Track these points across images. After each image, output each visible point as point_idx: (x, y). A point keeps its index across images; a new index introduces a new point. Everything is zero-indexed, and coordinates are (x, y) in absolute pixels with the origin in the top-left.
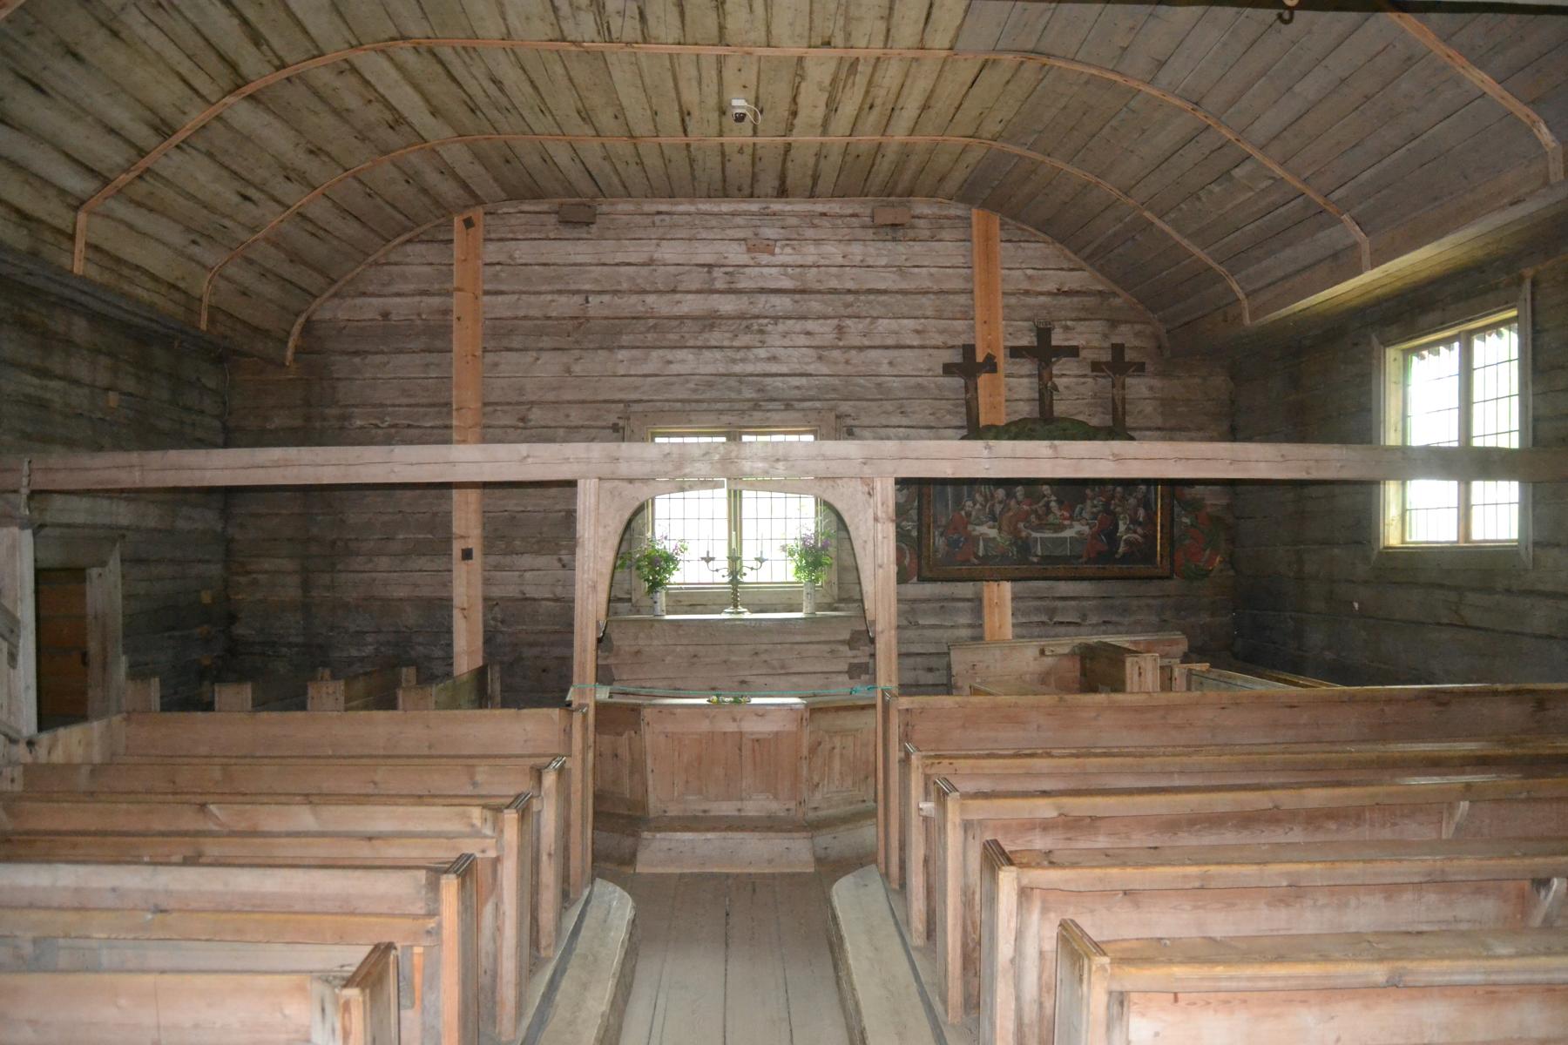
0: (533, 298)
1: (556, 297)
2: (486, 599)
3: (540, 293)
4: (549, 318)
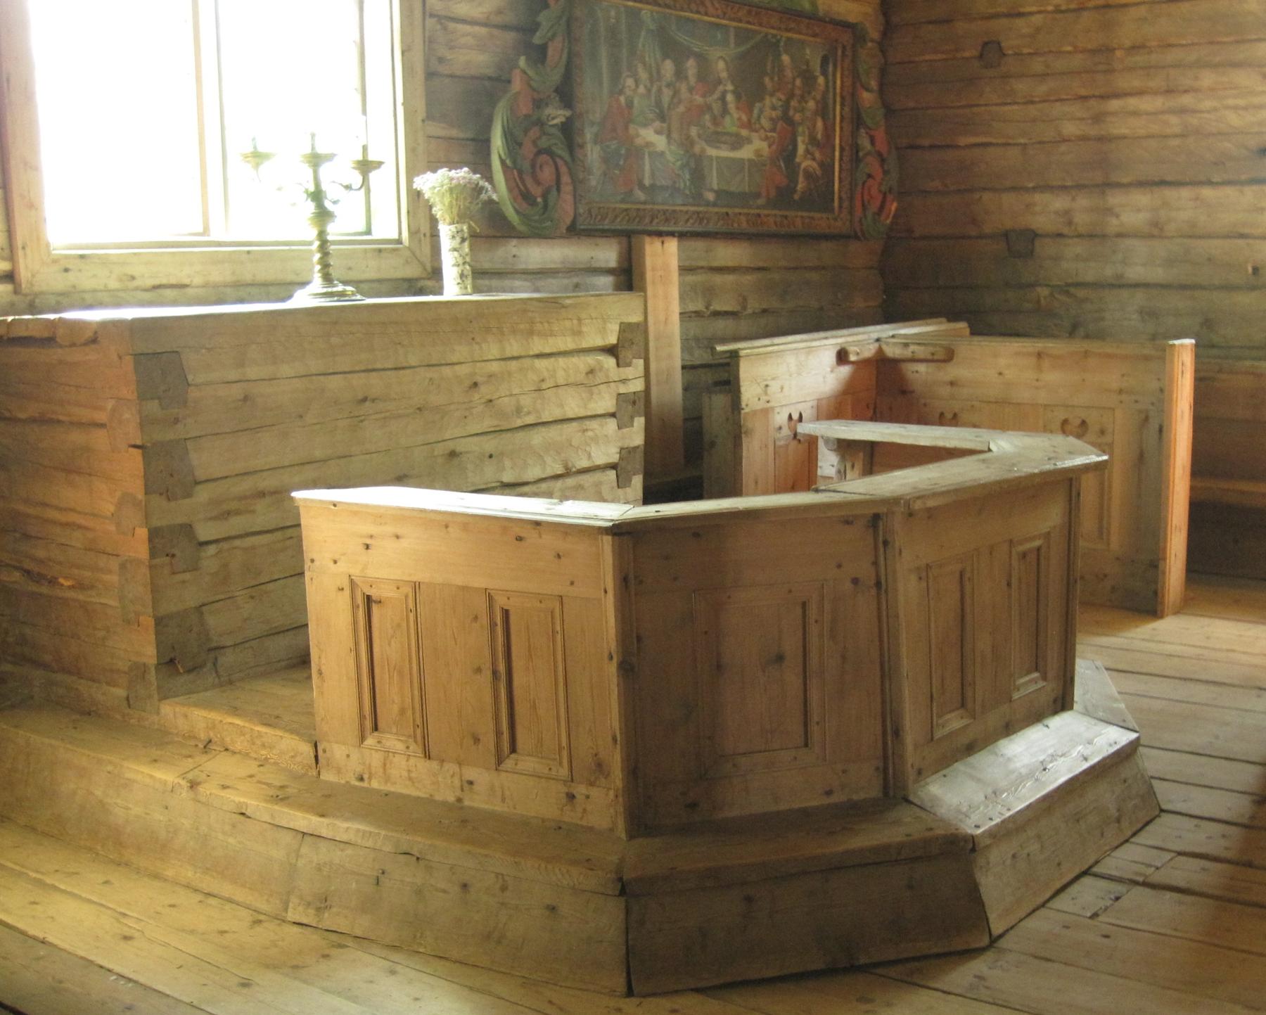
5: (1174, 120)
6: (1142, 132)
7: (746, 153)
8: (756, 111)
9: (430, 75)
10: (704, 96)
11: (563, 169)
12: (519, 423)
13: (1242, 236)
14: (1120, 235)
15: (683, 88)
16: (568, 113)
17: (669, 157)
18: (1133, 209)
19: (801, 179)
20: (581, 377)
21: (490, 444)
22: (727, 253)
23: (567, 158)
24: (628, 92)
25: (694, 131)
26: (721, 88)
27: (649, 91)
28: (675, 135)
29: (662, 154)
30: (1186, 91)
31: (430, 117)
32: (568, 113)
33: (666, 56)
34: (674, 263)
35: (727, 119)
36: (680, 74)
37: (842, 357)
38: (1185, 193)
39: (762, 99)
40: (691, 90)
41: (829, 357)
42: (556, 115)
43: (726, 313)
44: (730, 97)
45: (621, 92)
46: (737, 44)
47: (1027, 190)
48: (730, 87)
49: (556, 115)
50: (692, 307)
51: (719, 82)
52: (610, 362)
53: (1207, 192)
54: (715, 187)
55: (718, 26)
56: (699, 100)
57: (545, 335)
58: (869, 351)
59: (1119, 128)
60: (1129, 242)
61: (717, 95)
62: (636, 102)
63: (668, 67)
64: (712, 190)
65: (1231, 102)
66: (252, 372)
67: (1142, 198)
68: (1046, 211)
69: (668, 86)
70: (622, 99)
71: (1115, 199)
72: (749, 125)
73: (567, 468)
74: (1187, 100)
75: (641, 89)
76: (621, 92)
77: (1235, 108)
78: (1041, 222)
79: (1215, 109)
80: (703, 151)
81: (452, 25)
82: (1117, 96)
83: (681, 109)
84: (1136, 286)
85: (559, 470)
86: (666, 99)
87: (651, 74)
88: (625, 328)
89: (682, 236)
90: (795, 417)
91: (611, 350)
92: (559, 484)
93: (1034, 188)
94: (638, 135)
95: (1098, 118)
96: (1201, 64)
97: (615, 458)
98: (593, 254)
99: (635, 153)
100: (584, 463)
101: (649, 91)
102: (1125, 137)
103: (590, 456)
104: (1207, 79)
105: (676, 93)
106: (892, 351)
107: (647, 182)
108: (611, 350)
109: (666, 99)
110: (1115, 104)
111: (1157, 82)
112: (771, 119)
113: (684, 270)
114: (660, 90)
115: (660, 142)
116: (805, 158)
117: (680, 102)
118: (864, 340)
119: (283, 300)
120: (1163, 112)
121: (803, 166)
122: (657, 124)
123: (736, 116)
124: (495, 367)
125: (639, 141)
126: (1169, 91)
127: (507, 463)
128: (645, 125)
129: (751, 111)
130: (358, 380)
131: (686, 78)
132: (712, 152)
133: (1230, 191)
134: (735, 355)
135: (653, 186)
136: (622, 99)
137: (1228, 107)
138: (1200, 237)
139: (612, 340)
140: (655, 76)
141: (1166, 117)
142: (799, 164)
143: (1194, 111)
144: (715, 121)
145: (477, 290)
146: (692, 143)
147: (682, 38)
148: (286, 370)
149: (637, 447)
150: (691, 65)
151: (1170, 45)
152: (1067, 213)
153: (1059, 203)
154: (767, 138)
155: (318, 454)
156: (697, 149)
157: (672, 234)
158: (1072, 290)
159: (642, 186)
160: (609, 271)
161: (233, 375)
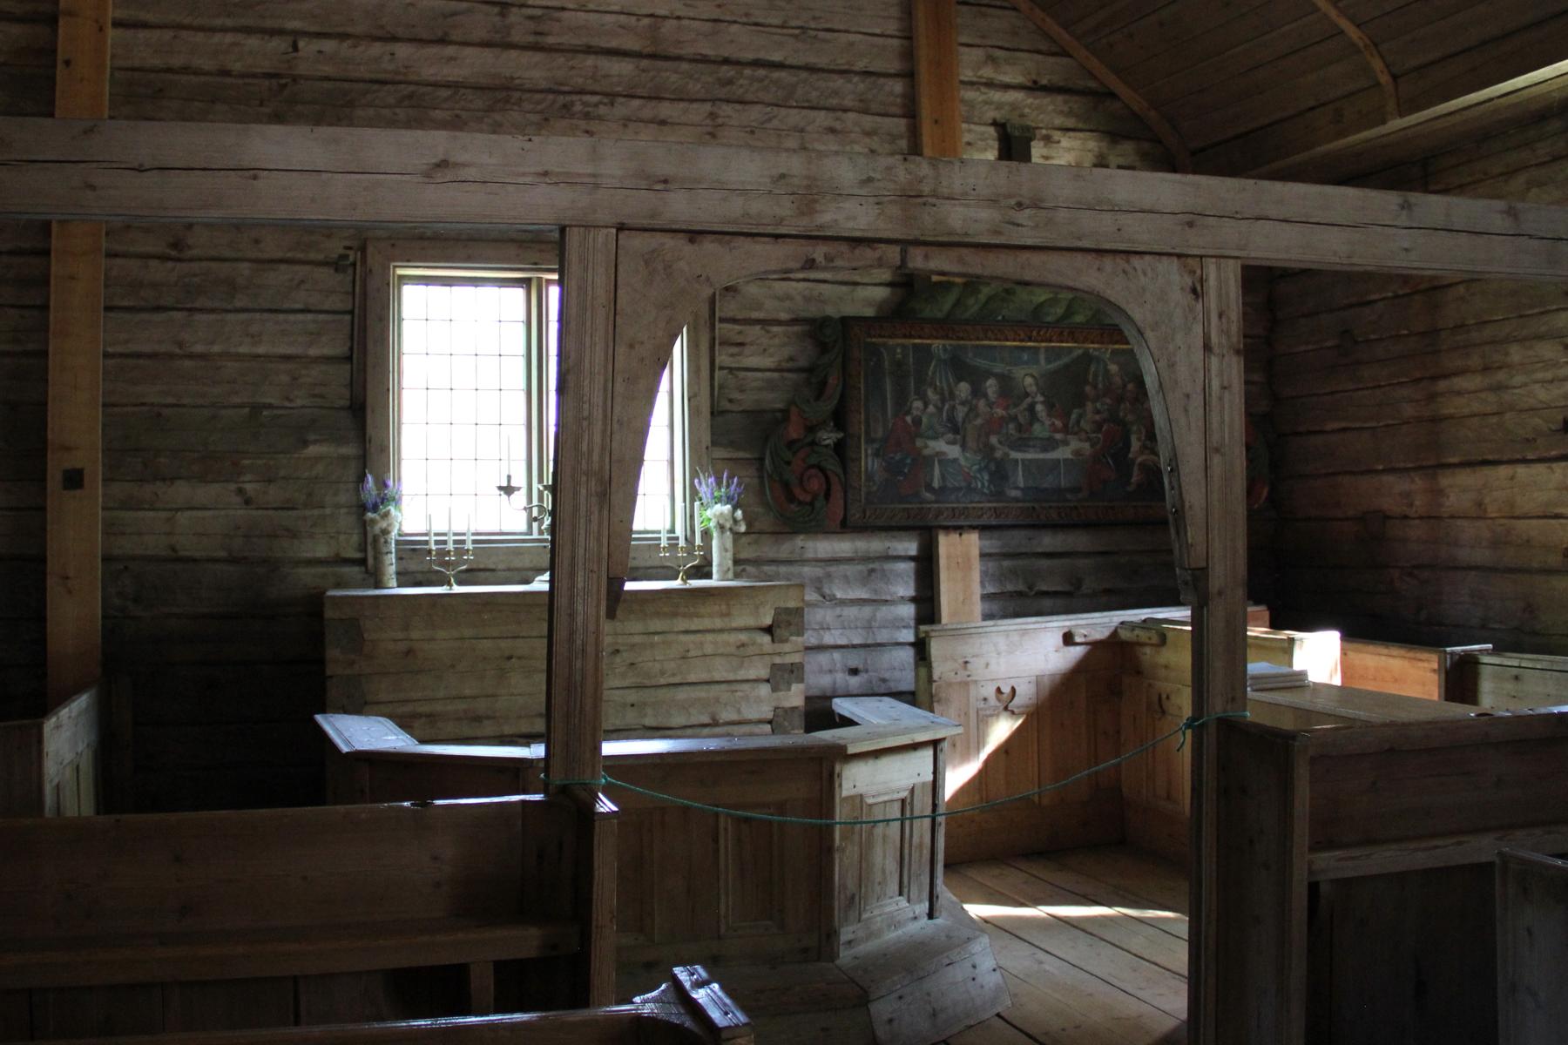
0: (200, 37)
1: (240, 37)
2: (107, 559)
3: (213, 30)
4: (226, 73)
5: (1491, 397)
6: (1466, 411)
7: (1063, 453)
8: (1074, 416)
9: (715, 413)
10: (1006, 408)
11: (834, 480)
12: (662, 681)
13: (1557, 516)
14: (1452, 517)
15: (982, 404)
16: (841, 435)
17: (963, 462)
18: (1460, 488)
19: (1136, 471)
20: (733, 650)
21: (632, 696)
22: (1049, 541)
23: (839, 471)
24: (915, 412)
25: (994, 440)
26: (1029, 400)
27: (940, 410)
28: (971, 443)
29: (955, 460)
30: (1500, 368)
31: (714, 443)
32: (841, 435)
33: (959, 379)
34: (975, 552)
35: (1037, 427)
36: (977, 392)
37: (1068, 639)
38: (1503, 471)
39: (1082, 405)
40: (990, 405)
41: (1058, 639)
42: (828, 437)
43: (1055, 594)
44: (1039, 407)
45: (908, 412)
46: (1048, 361)
47: (1377, 472)
48: (1040, 398)
49: (828, 437)
50: (991, 589)
51: (1027, 395)
52: (767, 638)
53: (1521, 471)
54: (1022, 485)
55: (1023, 349)
56: (1000, 412)
57: (691, 616)
58: (1100, 634)
59: (1450, 407)
60: (1459, 522)
61: (1024, 405)
62: (925, 420)
63: (964, 389)
64: (1017, 488)
65: (1540, 375)
66: (415, 635)
67: (1465, 478)
68: (1396, 492)
69: (963, 403)
70: (909, 419)
71: (1445, 481)
72: (1066, 429)
73: (714, 719)
74: (1501, 376)
75: (931, 409)
76: (908, 412)
77: (1543, 382)
78: (1388, 504)
79: (1526, 385)
80: (1007, 455)
81: (742, 374)
82: (1446, 376)
83: (979, 421)
84: (1470, 568)
85: (706, 719)
86: (961, 412)
87: (942, 394)
88: (779, 612)
89: (983, 529)
90: (1006, 690)
91: (768, 630)
92: (706, 731)
93: (1383, 471)
94: (926, 446)
95: (1432, 397)
96: (1508, 340)
97: (770, 716)
98: (887, 544)
99: (924, 462)
100: (734, 717)
101: (940, 410)
102: (1452, 417)
103: (739, 711)
104: (1516, 354)
105: (973, 409)
106: (1125, 635)
107: (936, 484)
108: (768, 630)
109: (961, 412)
110: (1442, 385)
111: (1475, 361)
112: (1095, 422)
113: (983, 555)
114: (953, 408)
115: (954, 452)
116: (1141, 452)
117: (977, 416)
118: (1098, 624)
119: (528, 582)
120: (1481, 391)
121: (1139, 460)
122: (950, 436)
123: (1048, 423)
124: (637, 639)
125: (926, 452)
126: (1486, 369)
127: (649, 711)
128: (935, 438)
129: (1069, 415)
130: (503, 644)
131: (985, 395)
132: (1014, 455)
133: (1540, 468)
134: (1292, 641)
135: (943, 489)
136: (909, 419)
137: (1536, 382)
138: (1518, 518)
139: (768, 621)
140: (948, 396)
141: (1483, 395)
142: (1133, 461)
143: (1507, 387)
144: (1020, 428)
145: (737, 576)
146: (993, 449)
147: (981, 363)
148: (441, 634)
149: (794, 709)
150: (991, 386)
151: (1485, 322)
152: (1407, 495)
153: (1398, 484)
154: (1088, 439)
155: (467, 692)
156: (998, 454)
157: (973, 528)
158: (1416, 572)
159: (929, 488)
160: (911, 558)
161: (400, 635)
